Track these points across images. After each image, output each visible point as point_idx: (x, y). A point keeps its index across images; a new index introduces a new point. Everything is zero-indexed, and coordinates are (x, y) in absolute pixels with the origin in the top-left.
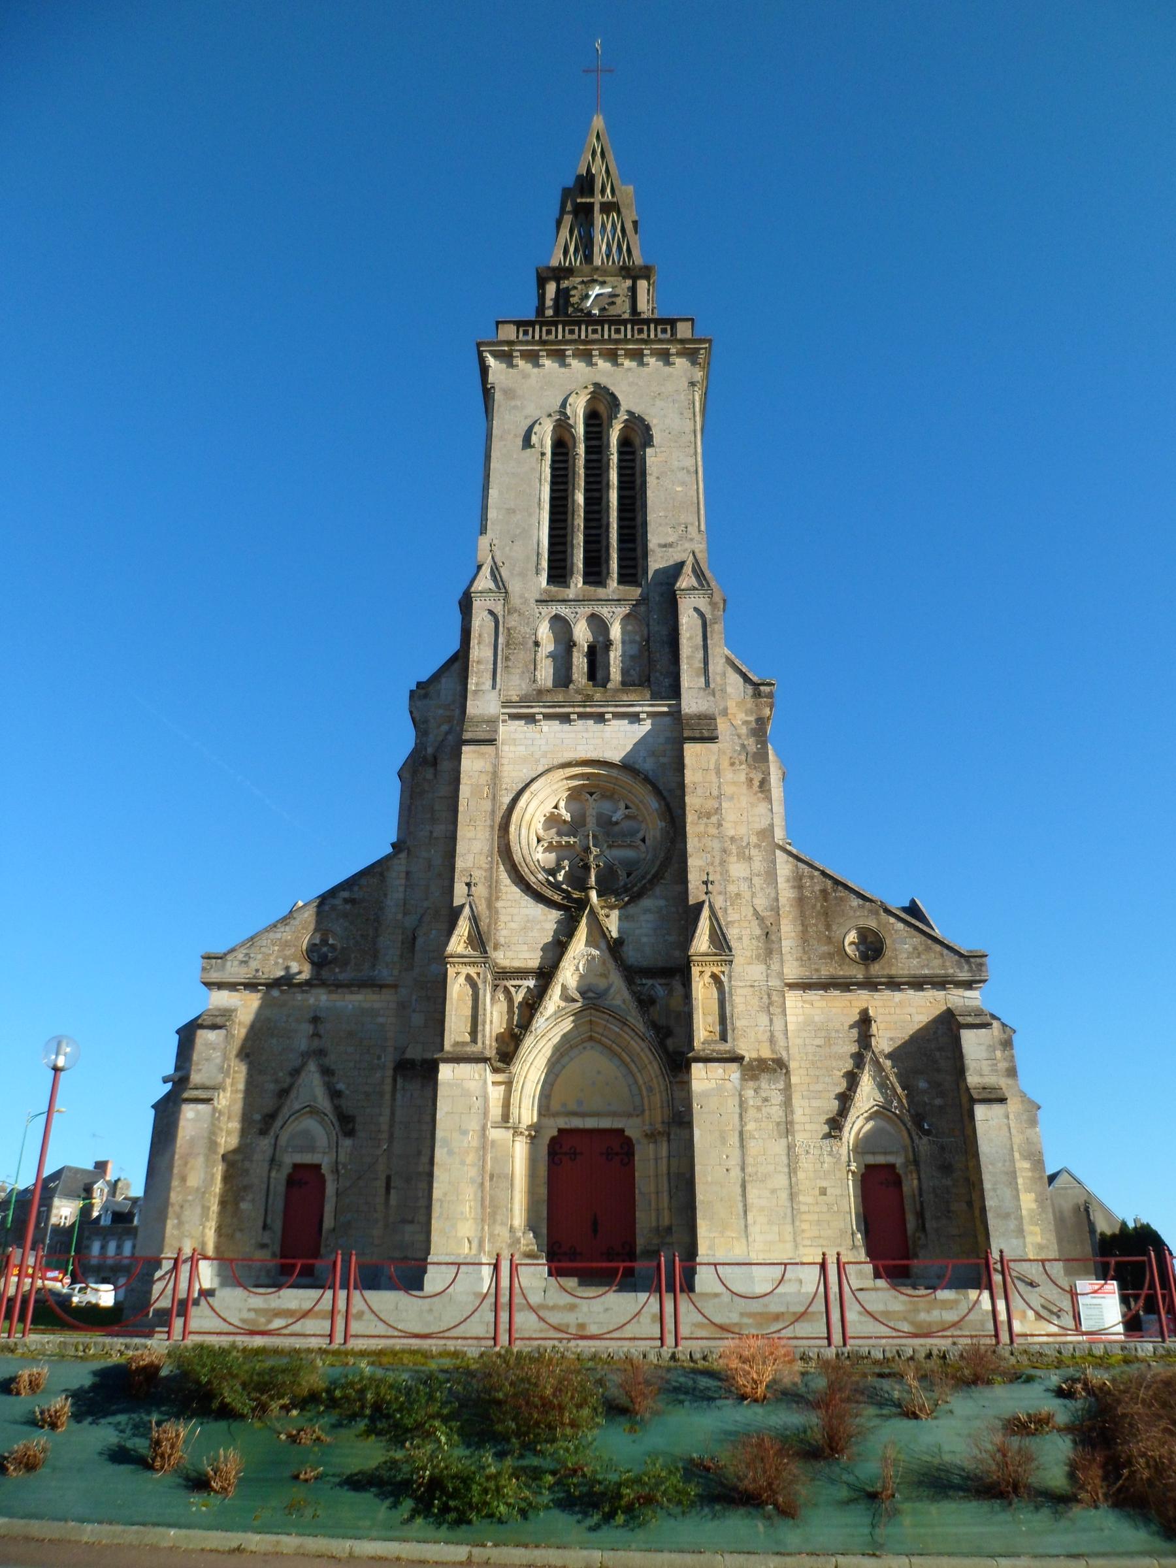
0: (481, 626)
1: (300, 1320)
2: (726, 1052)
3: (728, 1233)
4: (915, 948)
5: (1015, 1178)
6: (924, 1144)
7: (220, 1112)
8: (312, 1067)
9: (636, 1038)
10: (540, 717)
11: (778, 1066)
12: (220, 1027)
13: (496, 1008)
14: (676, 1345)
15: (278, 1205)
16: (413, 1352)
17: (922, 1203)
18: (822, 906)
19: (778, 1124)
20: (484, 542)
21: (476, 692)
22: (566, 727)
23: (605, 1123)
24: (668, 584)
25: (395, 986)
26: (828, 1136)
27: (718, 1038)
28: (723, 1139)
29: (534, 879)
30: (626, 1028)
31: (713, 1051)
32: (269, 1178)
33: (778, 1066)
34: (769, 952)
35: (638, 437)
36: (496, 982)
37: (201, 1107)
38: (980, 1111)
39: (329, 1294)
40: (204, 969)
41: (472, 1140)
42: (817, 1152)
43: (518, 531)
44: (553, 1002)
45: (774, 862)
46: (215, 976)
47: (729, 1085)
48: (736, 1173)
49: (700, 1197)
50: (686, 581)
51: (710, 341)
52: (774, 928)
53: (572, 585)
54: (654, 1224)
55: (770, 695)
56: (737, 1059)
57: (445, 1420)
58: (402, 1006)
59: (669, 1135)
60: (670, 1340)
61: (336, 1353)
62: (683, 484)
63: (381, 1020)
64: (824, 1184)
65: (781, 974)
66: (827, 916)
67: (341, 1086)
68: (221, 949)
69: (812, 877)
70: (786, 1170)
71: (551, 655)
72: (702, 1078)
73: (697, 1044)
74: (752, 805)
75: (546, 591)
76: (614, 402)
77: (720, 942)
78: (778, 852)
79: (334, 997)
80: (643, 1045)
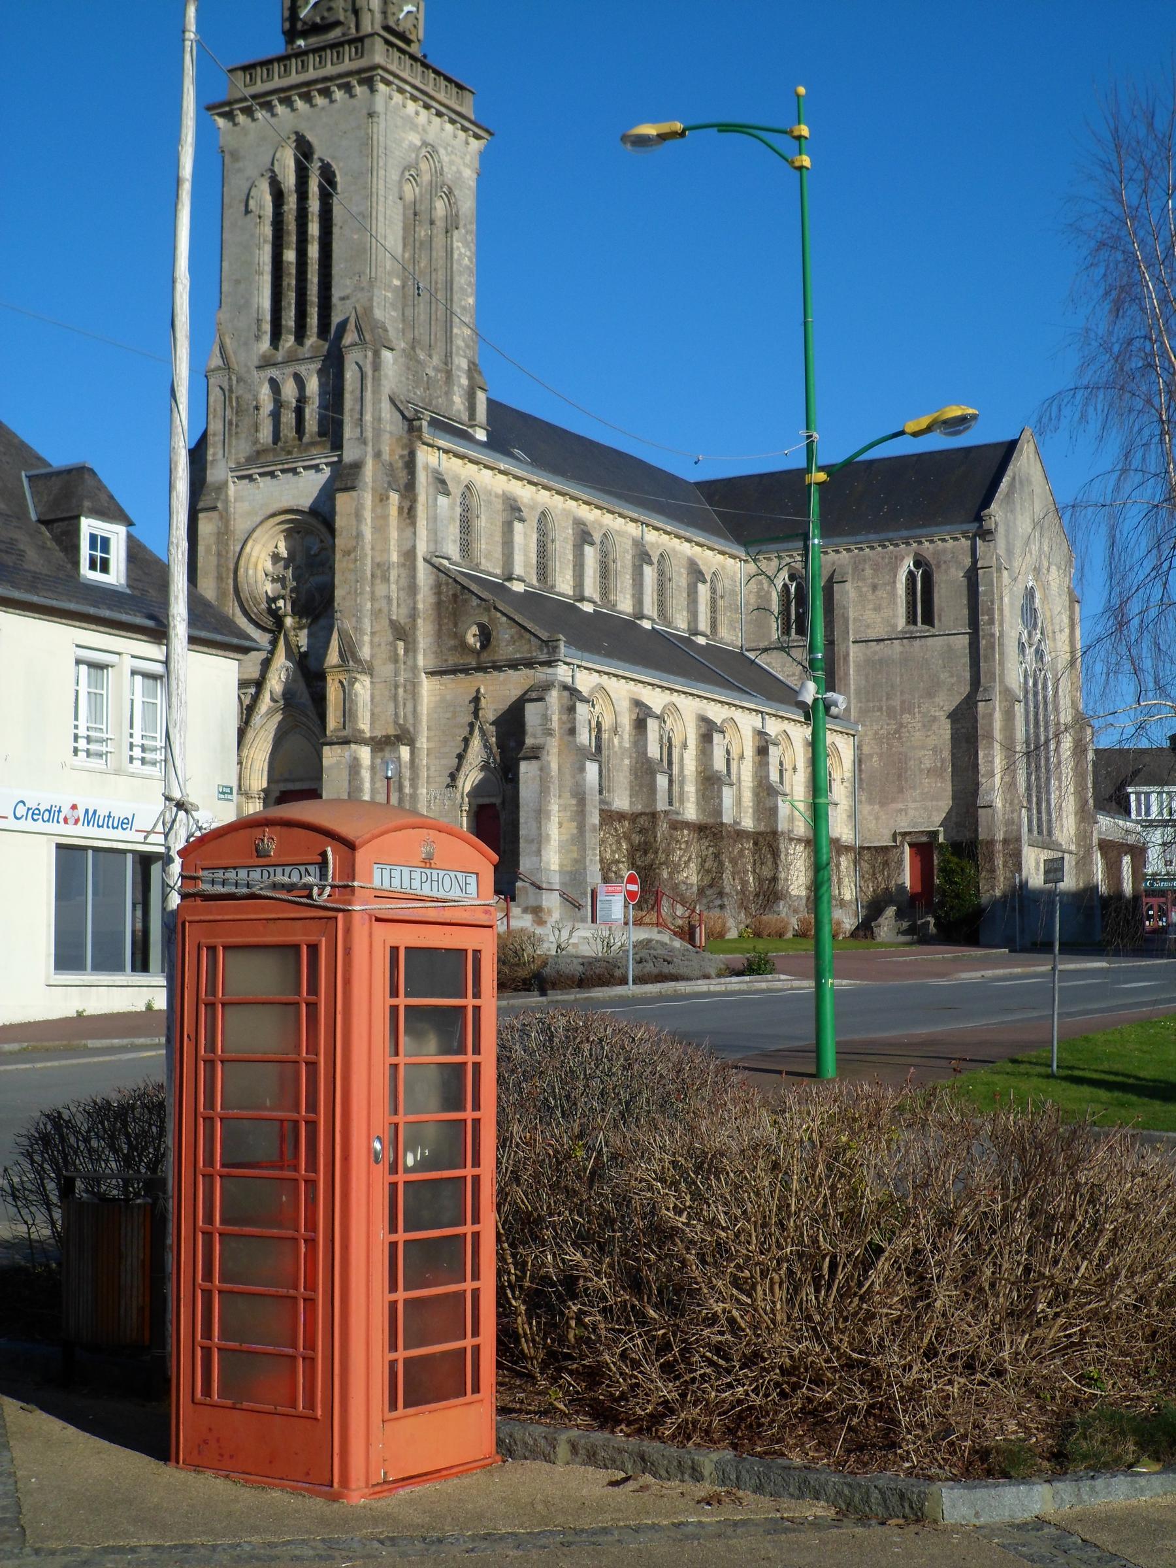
0: (215, 401)
26: (448, 786)
43: (243, 301)
44: (265, 704)
47: (343, 760)
50: (350, 337)
69: (447, 584)
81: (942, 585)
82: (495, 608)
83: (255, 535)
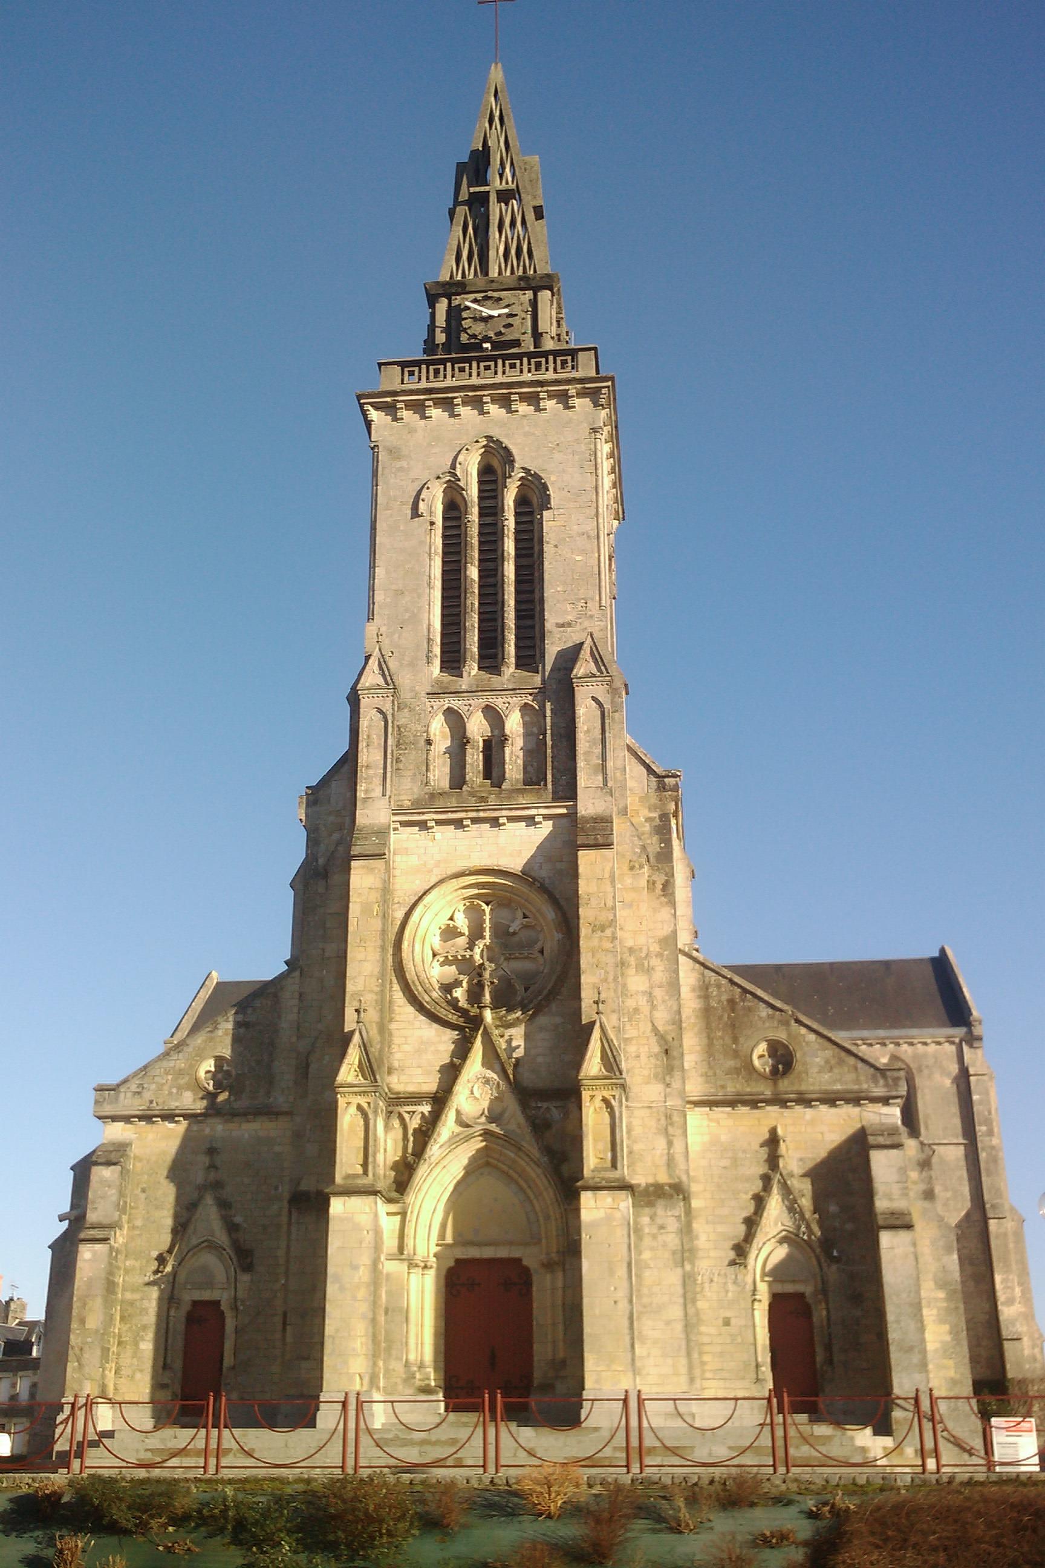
0: (369, 727)
1: (186, 1456)
2: (618, 1180)
3: (615, 1367)
4: (827, 1062)
5: (920, 1309)
6: (833, 1272)
7: (118, 1252)
8: (209, 1200)
9: (531, 1163)
10: (433, 824)
11: (677, 1191)
12: (115, 1164)
13: (391, 1136)
14: (497, 1472)
15: (179, 1343)
16: (273, 1480)
17: (830, 1335)
18: (729, 1017)
19: (674, 1253)
20: (371, 629)
21: (365, 800)
22: (460, 832)
23: (502, 1253)
24: (565, 669)
25: (289, 1113)
26: (733, 1263)
27: (609, 1165)
28: (611, 1272)
29: (427, 998)
30: (521, 1153)
31: (603, 1179)
32: (168, 1316)
33: (677, 1191)
34: (670, 1069)
35: (534, 499)
36: (390, 1109)
37: (98, 1247)
38: (886, 1239)
39: (203, 1431)
40: (97, 1102)
41: (363, 1274)
42: (722, 1280)
43: (407, 615)
44: (448, 1127)
45: (676, 972)
46: (108, 1109)
47: (618, 1215)
48: (623, 1305)
49: (587, 1329)
50: (583, 667)
51: (612, 379)
52: (676, 1043)
53: (465, 674)
54: (550, 1358)
55: (676, 788)
56: (625, 1186)
57: (289, 1532)
58: (298, 1135)
59: (564, 1265)
60: (491, 1469)
61: (209, 1481)
62: (583, 552)
63: (277, 1149)
64: (728, 1314)
65: (682, 1093)
66: (734, 1029)
67: (238, 1219)
68: (114, 1080)
69: (719, 986)
70: (681, 1300)
71: (448, 751)
72: (592, 1207)
73: (587, 1173)
74: (655, 910)
75: (438, 682)
76: (508, 458)
77: (611, 1062)
78: (682, 959)
79: (231, 1126)
80: (539, 1171)
81: (926, 1091)
82: (797, 1021)
83: (427, 899)
